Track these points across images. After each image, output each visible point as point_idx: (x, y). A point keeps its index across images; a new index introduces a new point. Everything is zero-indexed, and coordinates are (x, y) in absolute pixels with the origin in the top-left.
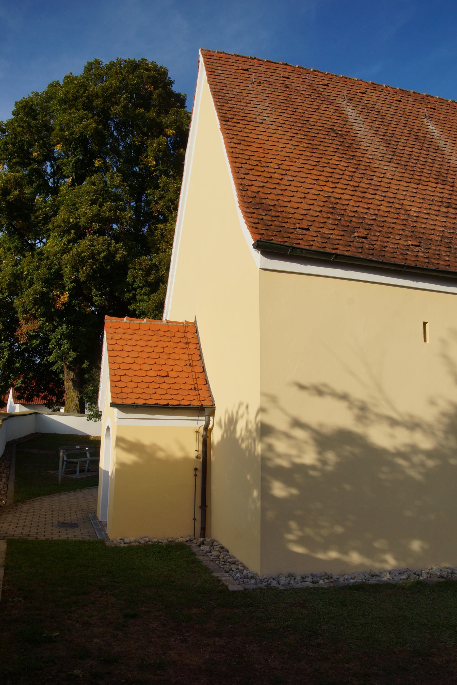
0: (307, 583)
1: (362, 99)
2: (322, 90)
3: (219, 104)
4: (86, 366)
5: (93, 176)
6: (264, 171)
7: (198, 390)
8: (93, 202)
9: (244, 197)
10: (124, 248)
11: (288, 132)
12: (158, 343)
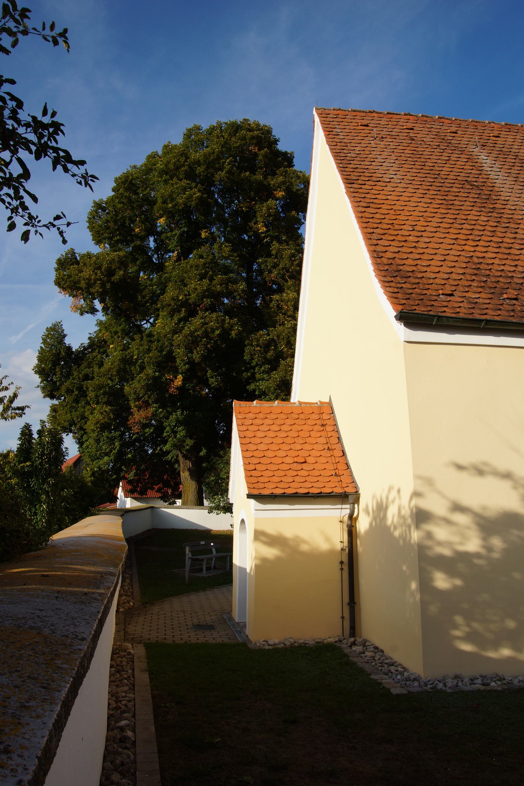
0: (476, 685)
1: (496, 143)
2: (451, 138)
3: (341, 166)
4: (203, 453)
5: (201, 248)
6: (398, 234)
7: (340, 476)
8: (202, 277)
9: (379, 265)
10: (239, 324)
11: (419, 189)
12: (292, 427)
